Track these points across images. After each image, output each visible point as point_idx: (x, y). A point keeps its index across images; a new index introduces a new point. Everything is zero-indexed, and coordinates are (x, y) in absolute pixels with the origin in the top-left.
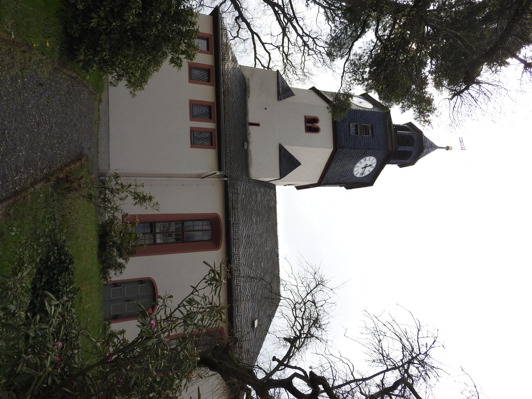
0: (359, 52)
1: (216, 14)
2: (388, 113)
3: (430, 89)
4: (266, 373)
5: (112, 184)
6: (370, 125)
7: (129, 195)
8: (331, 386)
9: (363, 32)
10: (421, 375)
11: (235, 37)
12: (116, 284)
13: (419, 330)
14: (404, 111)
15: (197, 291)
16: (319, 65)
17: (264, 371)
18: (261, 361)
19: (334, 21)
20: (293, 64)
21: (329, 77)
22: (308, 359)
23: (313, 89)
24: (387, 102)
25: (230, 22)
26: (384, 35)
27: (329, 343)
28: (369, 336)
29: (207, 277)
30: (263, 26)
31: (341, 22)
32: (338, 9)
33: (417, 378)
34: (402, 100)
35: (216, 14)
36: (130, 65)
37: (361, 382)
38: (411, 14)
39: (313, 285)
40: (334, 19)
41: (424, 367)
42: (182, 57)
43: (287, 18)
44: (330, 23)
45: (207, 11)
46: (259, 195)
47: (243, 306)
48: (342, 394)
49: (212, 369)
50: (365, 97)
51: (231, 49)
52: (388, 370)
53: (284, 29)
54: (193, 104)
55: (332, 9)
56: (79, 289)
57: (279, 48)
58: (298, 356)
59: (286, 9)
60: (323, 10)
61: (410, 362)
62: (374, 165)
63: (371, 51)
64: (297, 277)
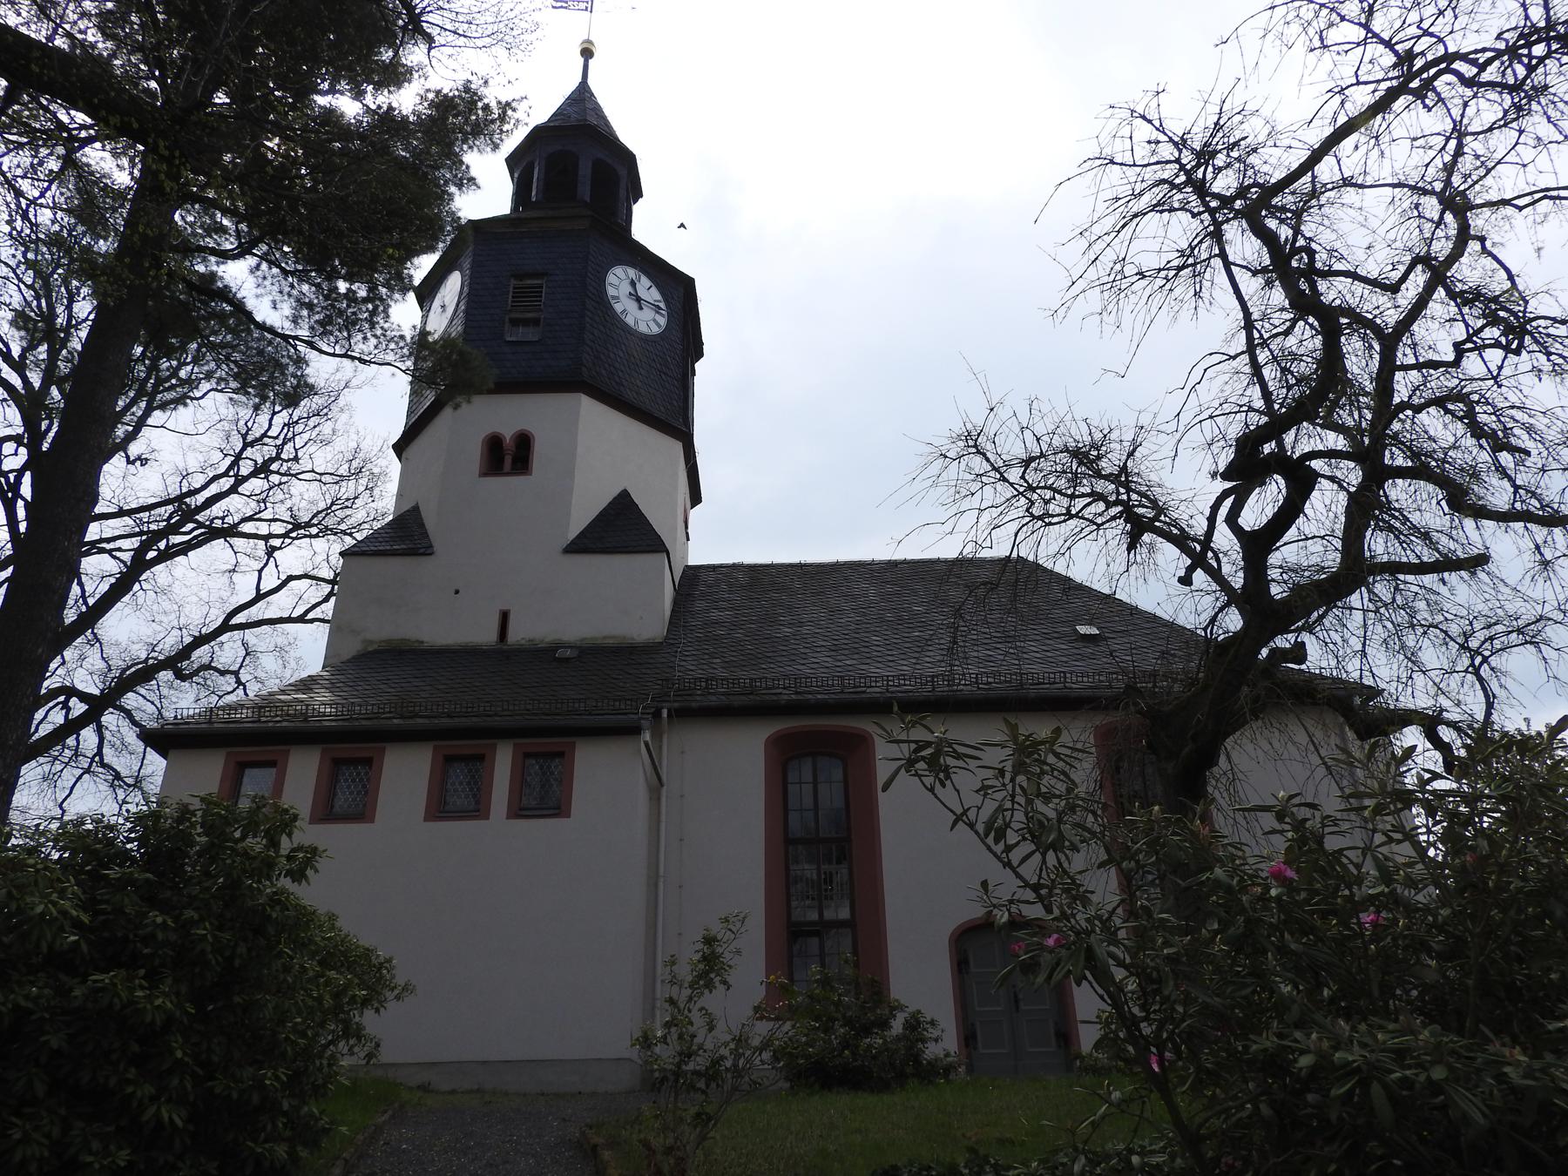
0: (287, 309)
1: (162, 739)
2: (473, 224)
3: (406, 100)
4: (1227, 605)
5: (666, 1054)
6: (513, 282)
7: (698, 1005)
8: (1265, 419)
9: (225, 294)
10: (1239, 160)
11: (239, 682)
12: (968, 1038)
13: (1112, 162)
14: (472, 180)
15: (965, 812)
16: (327, 428)
17: (1221, 609)
18: (1192, 618)
19: (191, 383)
20: (322, 506)
21: (365, 404)
22: (1189, 482)
23: (400, 448)
24: (442, 229)
25: (191, 696)
26: (237, 231)
27: (1145, 420)
28: (1127, 304)
29: (928, 781)
30: (204, 595)
31: (195, 361)
32: (154, 368)
33: (1250, 172)
34: (438, 186)
35: (162, 739)
36: (310, 1002)
37: (1256, 335)
38: (166, 153)
39: (978, 464)
40: (182, 382)
41: (1214, 154)
42: (285, 844)
43: (181, 523)
44: (198, 394)
45: (156, 764)
46: (715, 615)
47: (1036, 668)
48: (1289, 388)
49: (1212, 761)
50: (426, 293)
51: (271, 694)
52: (1223, 255)
53: (213, 533)
54: (439, 808)
55: (155, 386)
56: (972, 1150)
57: (275, 549)
58: (1181, 514)
59: (153, 527)
60: (157, 413)
61: (1201, 189)
62: (632, 272)
63: (285, 273)
64: (953, 510)
